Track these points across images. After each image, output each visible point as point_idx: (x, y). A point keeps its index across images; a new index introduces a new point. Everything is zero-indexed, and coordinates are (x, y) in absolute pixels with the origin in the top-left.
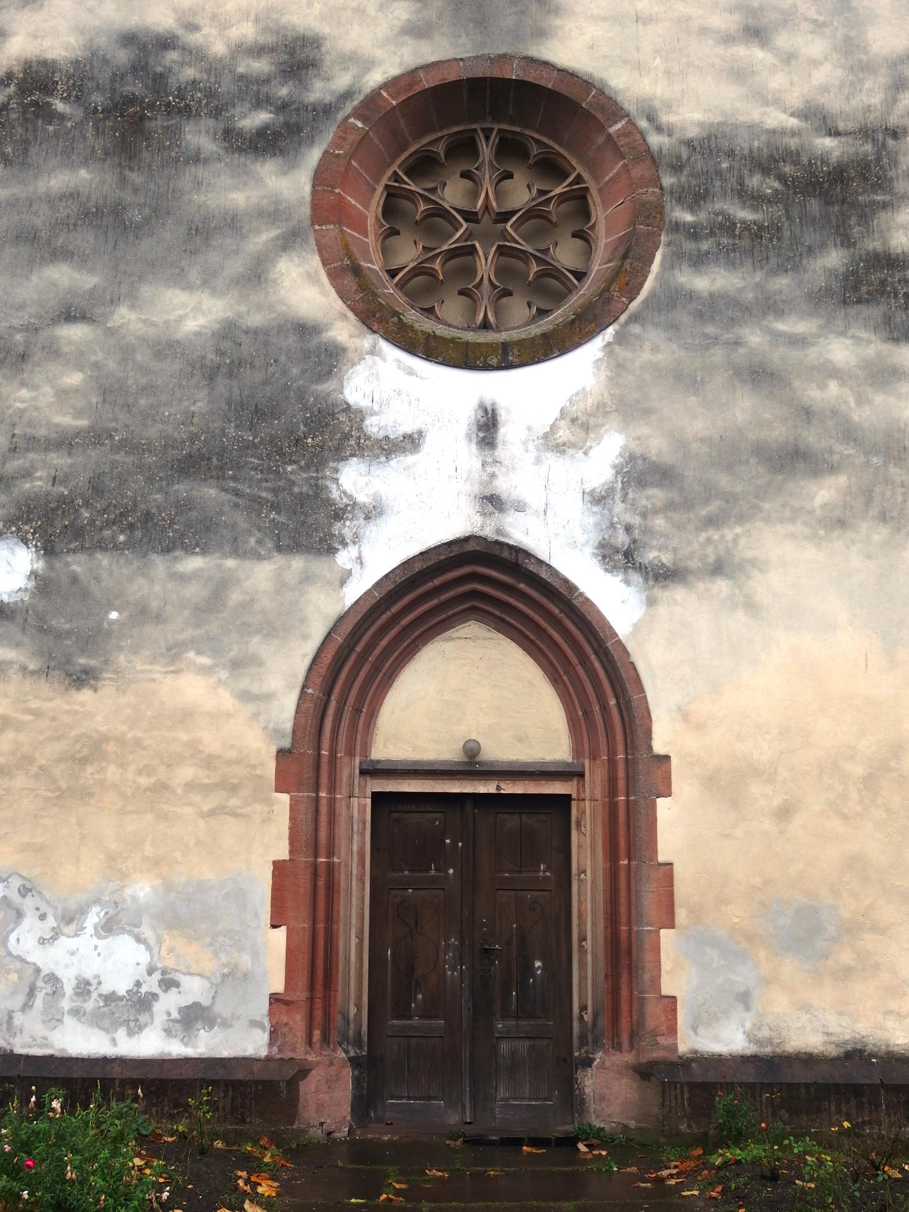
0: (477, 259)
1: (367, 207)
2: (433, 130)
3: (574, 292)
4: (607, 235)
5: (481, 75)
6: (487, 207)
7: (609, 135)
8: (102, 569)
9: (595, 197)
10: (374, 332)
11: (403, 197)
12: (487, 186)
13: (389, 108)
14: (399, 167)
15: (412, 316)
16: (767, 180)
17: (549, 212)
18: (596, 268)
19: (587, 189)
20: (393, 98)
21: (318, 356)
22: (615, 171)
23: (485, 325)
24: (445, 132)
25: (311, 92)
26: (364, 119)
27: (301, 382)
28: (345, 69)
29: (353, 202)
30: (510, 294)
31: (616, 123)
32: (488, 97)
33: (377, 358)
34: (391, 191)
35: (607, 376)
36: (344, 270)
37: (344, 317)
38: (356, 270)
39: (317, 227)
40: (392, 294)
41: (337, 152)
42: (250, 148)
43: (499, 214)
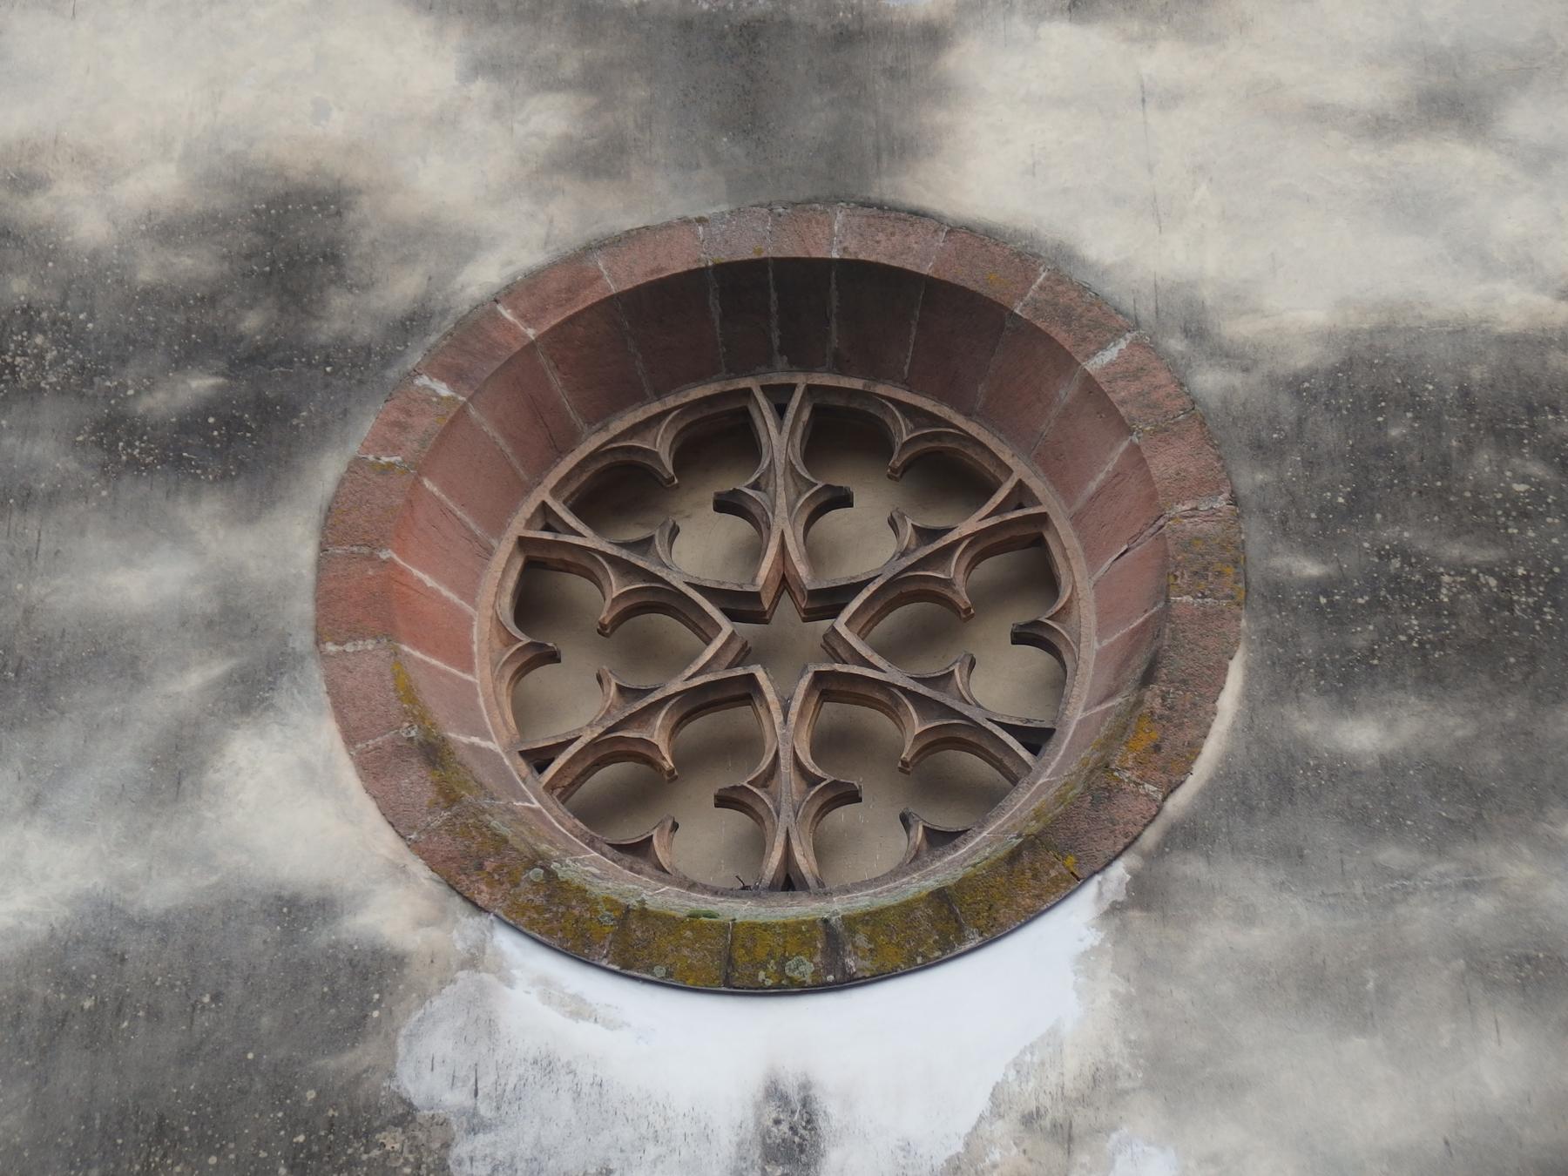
0: (762, 711)
1: (470, 595)
2: (639, 398)
3: (1023, 784)
4: (1102, 631)
5: (748, 254)
6: (785, 583)
7: (1088, 378)
9: (1065, 539)
10: (480, 909)
11: (568, 568)
12: (785, 525)
13: (517, 347)
14: (555, 492)
15: (592, 869)
16: (1516, 461)
17: (948, 583)
18: (1079, 715)
19: (1043, 519)
20: (529, 322)
21: (331, 980)
22: (1110, 467)
23: (789, 882)
24: (671, 401)
25: (317, 318)
26: (454, 376)
27: (281, 1053)
28: (406, 260)
29: (430, 582)
30: (853, 796)
31: (1102, 347)
32: (774, 309)
33: (487, 977)
34: (535, 554)
35: (1115, 994)
36: (401, 751)
37: (398, 872)
38: (434, 752)
39: (331, 648)
40: (536, 812)
41: (384, 459)
42: (163, 462)
43: (814, 594)
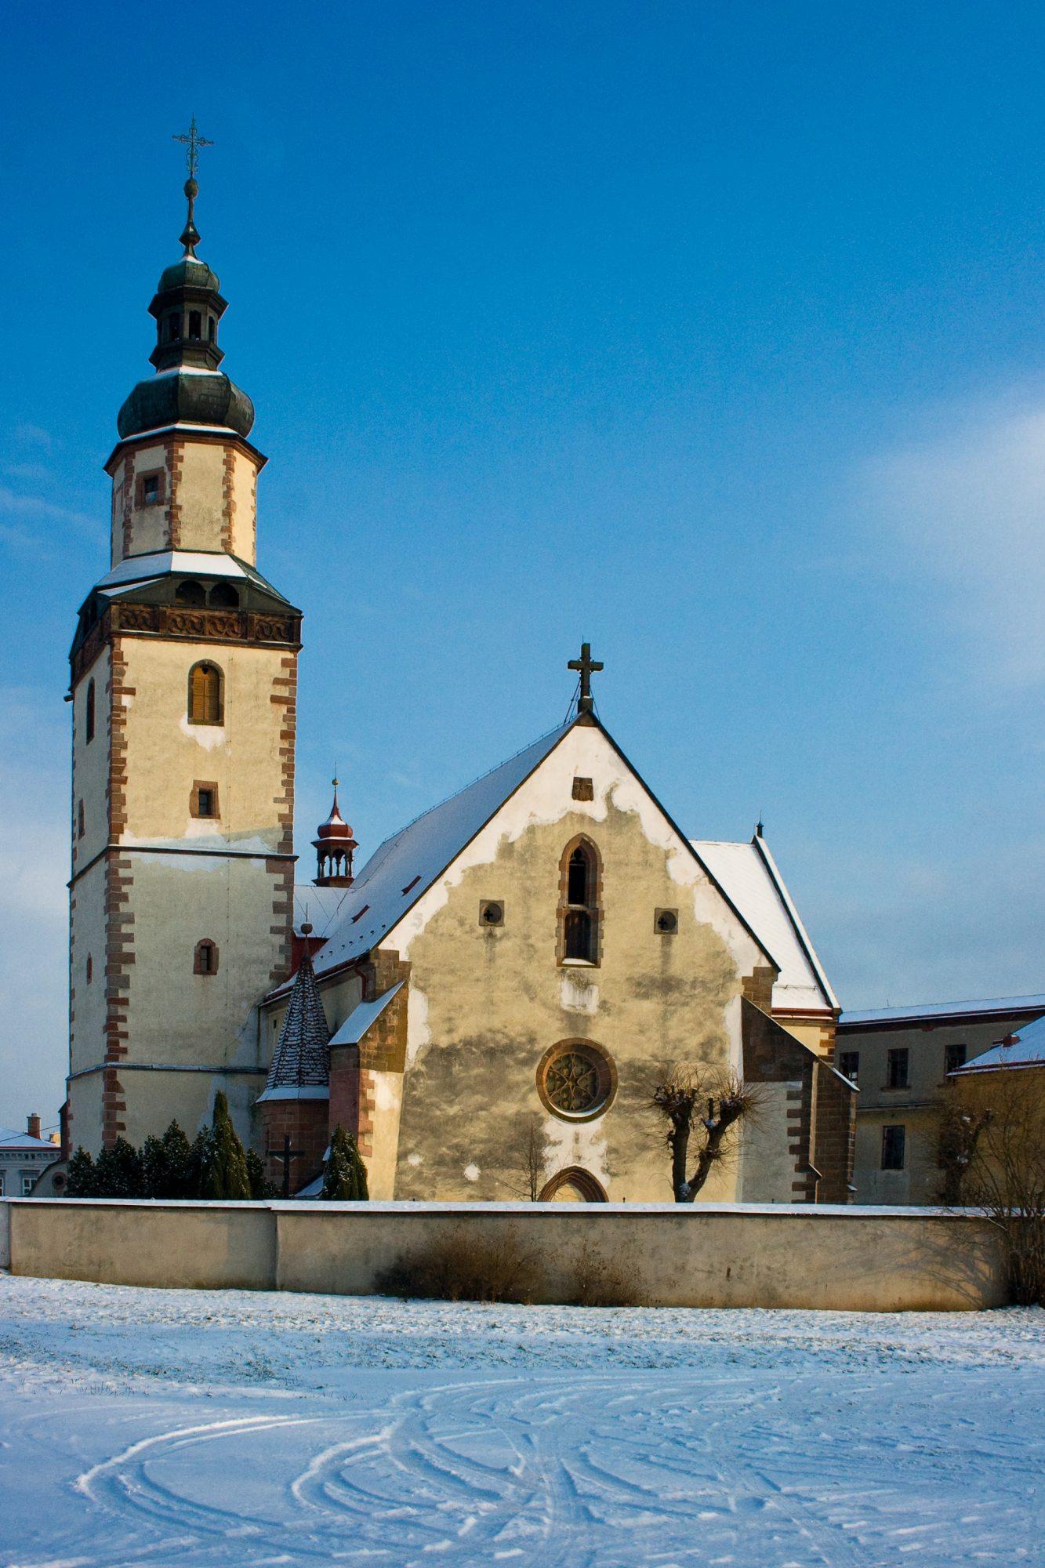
8: (496, 1173)
